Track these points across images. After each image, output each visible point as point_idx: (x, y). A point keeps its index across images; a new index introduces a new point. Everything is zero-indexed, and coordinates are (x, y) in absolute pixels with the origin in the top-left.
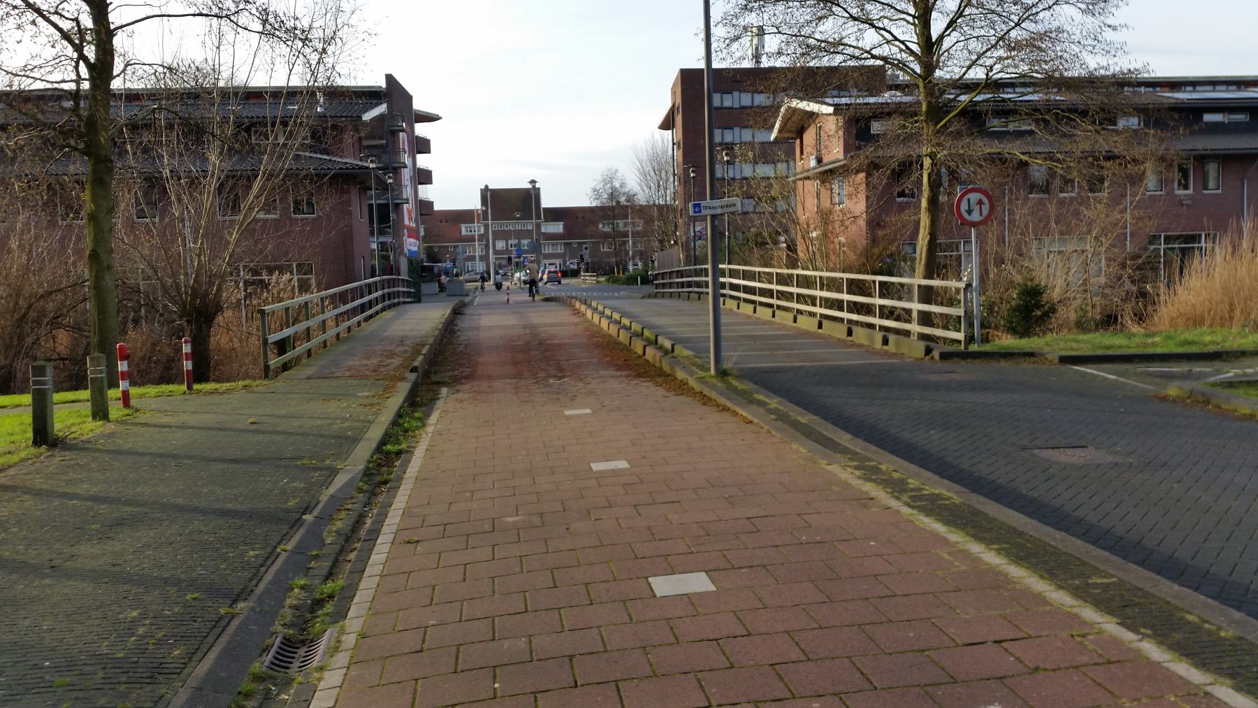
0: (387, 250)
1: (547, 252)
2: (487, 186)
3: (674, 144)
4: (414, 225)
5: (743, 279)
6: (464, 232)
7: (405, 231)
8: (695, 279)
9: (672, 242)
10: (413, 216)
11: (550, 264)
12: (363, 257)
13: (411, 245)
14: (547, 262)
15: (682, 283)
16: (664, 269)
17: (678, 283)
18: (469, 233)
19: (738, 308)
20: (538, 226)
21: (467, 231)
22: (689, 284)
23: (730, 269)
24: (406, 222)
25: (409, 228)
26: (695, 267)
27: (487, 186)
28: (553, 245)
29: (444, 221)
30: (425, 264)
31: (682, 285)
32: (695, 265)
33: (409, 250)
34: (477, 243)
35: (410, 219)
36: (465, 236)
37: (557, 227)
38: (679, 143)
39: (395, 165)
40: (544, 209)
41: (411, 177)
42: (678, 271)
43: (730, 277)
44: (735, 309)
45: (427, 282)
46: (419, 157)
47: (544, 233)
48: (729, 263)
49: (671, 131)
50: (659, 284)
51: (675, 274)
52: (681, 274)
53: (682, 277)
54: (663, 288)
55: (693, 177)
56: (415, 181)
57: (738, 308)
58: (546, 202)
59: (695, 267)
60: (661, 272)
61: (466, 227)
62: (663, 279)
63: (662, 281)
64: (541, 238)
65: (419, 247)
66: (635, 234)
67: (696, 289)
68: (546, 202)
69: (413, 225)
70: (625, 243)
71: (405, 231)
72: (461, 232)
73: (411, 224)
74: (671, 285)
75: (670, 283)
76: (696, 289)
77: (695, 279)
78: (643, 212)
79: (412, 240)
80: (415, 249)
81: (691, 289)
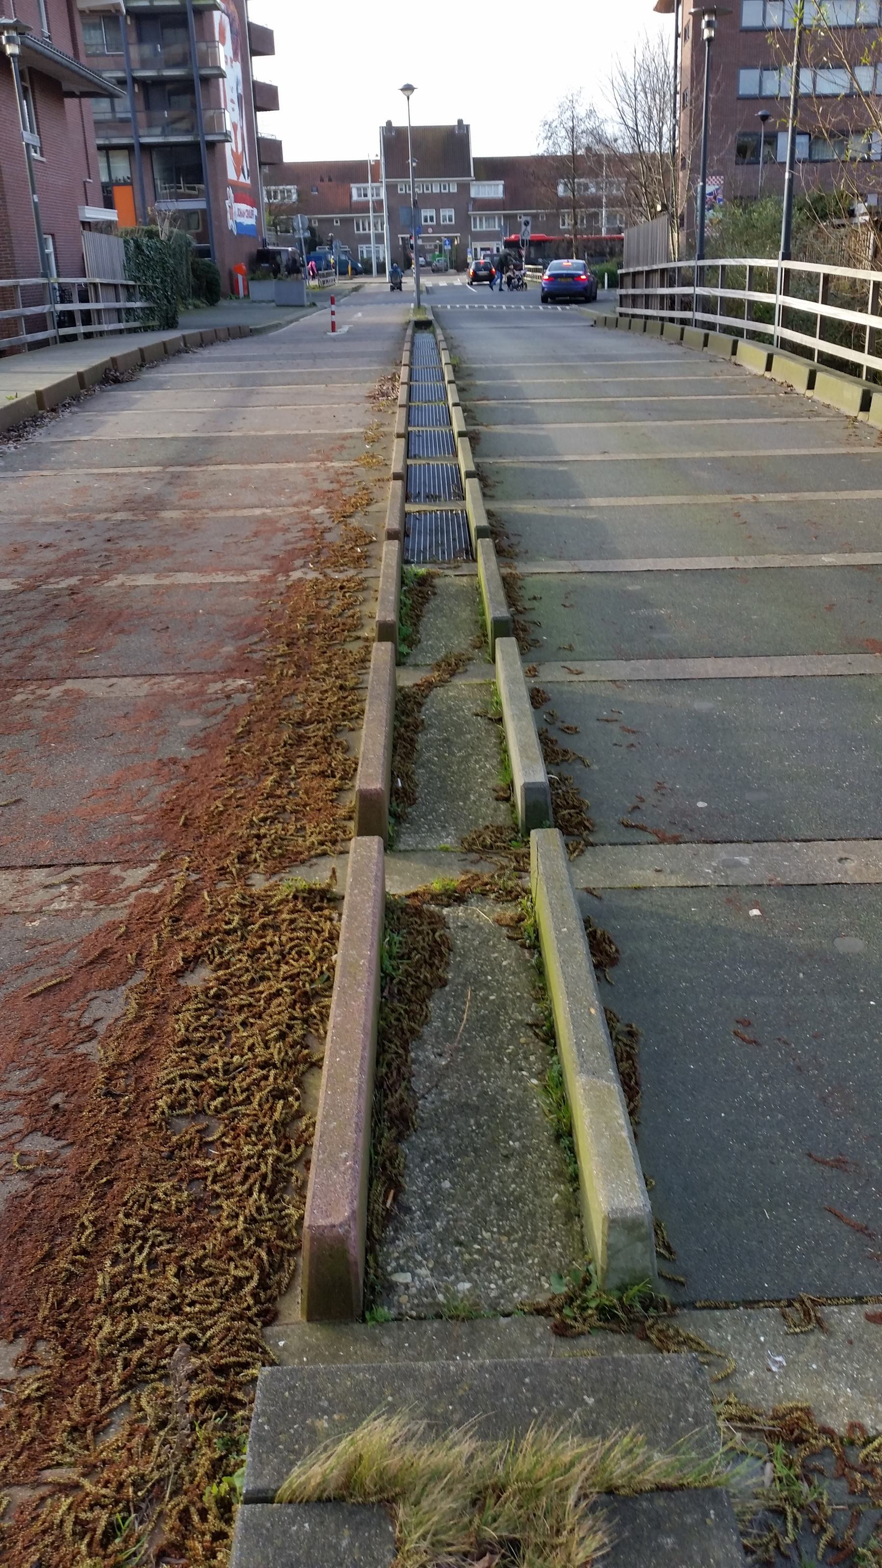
0: (154, 221)
1: (478, 229)
2: (389, 123)
3: (677, 35)
4: (248, 181)
5: (824, 302)
6: (355, 197)
7: (230, 191)
8: (700, 291)
9: (659, 208)
10: (246, 166)
11: (482, 249)
12: (53, 235)
13: (241, 215)
14: (478, 245)
15: (672, 297)
16: (638, 265)
17: (662, 296)
18: (363, 198)
19: (811, 385)
20: (464, 188)
21: (359, 195)
22: (686, 303)
23: (788, 271)
24: (232, 175)
25: (235, 186)
26: (701, 263)
27: (389, 123)
28: (488, 219)
29: (326, 179)
30: (270, 248)
31: (671, 302)
32: (701, 257)
33: (239, 225)
34: (371, 214)
35: (239, 170)
36: (357, 203)
37: (494, 190)
38: (686, 31)
39: (204, 72)
40: (476, 160)
41: (239, 97)
42: (663, 271)
43: (786, 293)
44: (801, 387)
45: (259, 279)
46: (257, 62)
47: (474, 200)
48: (787, 257)
49: (673, 15)
50: (626, 296)
51: (657, 278)
52: (668, 277)
53: (671, 285)
54: (634, 306)
55: (710, 40)
56: (248, 103)
57: (811, 385)
58: (479, 149)
59: (701, 263)
60: (631, 270)
61: (359, 189)
62: (634, 287)
63: (631, 291)
64: (470, 207)
65: (258, 219)
66: (613, 202)
67: (700, 316)
68: (479, 149)
69: (245, 180)
70: (595, 216)
71: (230, 191)
72: (351, 196)
73: (242, 179)
74: (647, 301)
75: (647, 296)
76: (700, 316)
77: (700, 291)
78: (618, 161)
79: (244, 207)
80: (252, 222)
81: (688, 315)
